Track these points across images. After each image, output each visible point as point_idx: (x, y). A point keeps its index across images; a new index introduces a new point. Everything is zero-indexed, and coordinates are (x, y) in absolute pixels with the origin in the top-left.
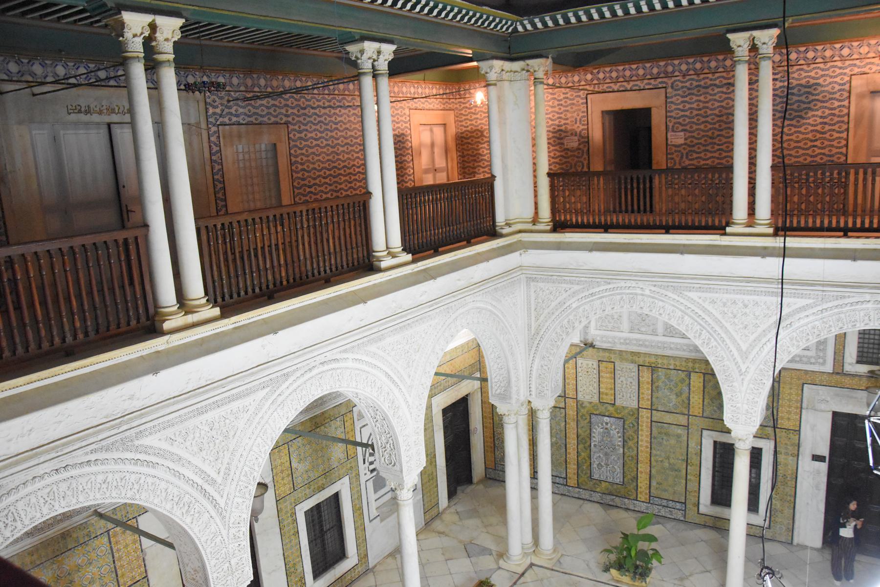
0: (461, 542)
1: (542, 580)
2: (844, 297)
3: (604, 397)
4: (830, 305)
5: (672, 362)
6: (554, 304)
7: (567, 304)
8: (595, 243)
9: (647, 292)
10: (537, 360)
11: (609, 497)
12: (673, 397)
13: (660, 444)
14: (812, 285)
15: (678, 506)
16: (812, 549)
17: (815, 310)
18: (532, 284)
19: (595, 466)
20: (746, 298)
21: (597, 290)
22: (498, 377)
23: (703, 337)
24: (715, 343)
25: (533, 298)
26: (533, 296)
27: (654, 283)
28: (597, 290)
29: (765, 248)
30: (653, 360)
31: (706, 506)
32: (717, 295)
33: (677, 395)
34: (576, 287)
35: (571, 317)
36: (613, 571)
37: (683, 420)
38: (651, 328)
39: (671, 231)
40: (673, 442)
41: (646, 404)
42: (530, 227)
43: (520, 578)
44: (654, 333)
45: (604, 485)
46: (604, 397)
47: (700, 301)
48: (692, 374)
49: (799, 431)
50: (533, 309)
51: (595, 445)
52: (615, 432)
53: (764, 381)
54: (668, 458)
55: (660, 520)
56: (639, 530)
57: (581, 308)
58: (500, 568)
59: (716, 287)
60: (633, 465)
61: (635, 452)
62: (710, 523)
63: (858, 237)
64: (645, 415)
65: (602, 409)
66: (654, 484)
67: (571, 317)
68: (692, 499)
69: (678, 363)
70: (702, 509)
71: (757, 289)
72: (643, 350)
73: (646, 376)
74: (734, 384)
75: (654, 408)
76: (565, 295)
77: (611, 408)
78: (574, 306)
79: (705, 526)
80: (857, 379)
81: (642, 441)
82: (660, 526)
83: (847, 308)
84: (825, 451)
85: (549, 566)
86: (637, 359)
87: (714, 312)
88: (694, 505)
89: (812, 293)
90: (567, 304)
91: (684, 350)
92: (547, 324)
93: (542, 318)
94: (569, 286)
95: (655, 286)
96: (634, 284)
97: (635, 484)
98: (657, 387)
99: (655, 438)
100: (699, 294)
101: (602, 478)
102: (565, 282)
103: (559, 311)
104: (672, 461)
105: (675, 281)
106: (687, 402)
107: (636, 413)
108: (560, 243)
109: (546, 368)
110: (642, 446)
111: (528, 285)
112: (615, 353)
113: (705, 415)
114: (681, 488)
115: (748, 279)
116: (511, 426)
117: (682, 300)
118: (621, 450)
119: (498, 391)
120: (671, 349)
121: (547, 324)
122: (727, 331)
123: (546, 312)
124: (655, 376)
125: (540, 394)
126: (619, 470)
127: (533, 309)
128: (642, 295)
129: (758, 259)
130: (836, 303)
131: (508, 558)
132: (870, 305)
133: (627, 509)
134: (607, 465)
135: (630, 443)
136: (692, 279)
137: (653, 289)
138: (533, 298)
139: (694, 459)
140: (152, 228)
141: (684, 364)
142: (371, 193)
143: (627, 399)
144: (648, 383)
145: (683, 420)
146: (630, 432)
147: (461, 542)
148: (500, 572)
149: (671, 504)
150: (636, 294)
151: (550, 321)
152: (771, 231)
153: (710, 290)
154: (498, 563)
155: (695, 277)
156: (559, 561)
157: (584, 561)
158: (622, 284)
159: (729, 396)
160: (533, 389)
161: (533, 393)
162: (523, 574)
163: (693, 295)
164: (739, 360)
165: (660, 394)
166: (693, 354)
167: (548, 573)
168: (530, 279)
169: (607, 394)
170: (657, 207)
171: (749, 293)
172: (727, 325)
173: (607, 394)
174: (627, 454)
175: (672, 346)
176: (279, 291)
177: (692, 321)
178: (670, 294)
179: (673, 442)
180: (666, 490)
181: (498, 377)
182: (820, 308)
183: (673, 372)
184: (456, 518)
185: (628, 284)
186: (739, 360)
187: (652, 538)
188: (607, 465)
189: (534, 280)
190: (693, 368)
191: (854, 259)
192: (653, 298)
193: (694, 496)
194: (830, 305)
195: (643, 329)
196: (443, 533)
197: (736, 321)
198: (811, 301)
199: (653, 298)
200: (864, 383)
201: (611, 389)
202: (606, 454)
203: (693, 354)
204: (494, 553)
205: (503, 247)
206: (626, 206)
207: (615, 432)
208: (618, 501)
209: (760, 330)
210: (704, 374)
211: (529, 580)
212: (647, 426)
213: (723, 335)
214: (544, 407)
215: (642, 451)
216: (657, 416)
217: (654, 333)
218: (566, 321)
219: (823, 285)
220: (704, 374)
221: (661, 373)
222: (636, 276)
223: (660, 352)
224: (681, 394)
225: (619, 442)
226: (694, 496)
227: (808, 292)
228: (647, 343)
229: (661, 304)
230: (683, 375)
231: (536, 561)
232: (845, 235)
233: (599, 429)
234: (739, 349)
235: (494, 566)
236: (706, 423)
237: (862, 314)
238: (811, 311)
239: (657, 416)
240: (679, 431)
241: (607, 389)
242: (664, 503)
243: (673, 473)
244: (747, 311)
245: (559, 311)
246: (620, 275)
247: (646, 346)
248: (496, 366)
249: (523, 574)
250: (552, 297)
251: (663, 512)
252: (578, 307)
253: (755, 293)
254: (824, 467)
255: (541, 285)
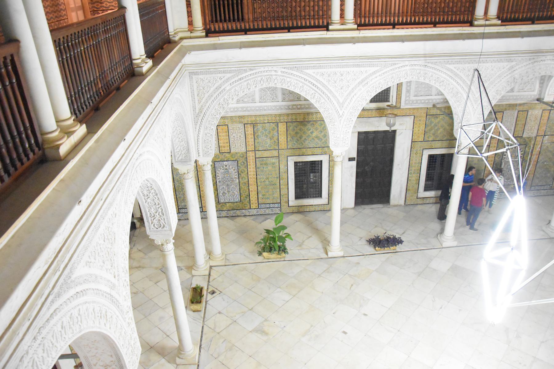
0: (156, 268)
1: (223, 273)
2: (396, 64)
3: (223, 149)
4: (388, 69)
5: (266, 118)
6: (212, 89)
7: (222, 88)
8: (241, 42)
9: (279, 73)
10: (202, 131)
11: (232, 212)
12: (268, 141)
13: (262, 171)
14: (379, 58)
15: (276, 205)
16: (352, 209)
17: (380, 73)
18: (194, 77)
19: (221, 194)
20: (342, 70)
21: (244, 75)
22: (179, 148)
23: (316, 97)
24: (323, 101)
25: (195, 87)
26: (195, 85)
27: (284, 66)
28: (244, 75)
29: (353, 38)
30: (254, 119)
31: (292, 201)
32: (325, 70)
33: (271, 139)
34: (229, 75)
35: (226, 97)
36: (265, 254)
37: (275, 153)
38: (251, 98)
39: (248, 33)
40: (270, 168)
41: (251, 148)
42: (188, 34)
43: (209, 278)
44: (253, 101)
45: (228, 205)
46: (223, 149)
47: (314, 75)
48: (279, 124)
49: (412, 142)
50: (196, 95)
51: (220, 182)
52: (232, 170)
53: (352, 119)
54: (268, 178)
55: (268, 217)
56: (276, 225)
57: (233, 90)
58: (193, 276)
59: (323, 65)
60: (246, 188)
61: (247, 180)
62: (296, 210)
63: (384, 29)
64: (251, 155)
65: (222, 157)
66: (260, 196)
67: (226, 97)
68: (284, 199)
69: (270, 119)
70: (291, 204)
71: (348, 64)
72: (246, 113)
73: (250, 130)
74: (335, 124)
75: (256, 149)
76: (220, 82)
77: (227, 155)
78: (228, 88)
79: (293, 213)
80: (370, 111)
81: (250, 171)
82: (269, 220)
83: (397, 70)
84: (354, 155)
85: (223, 264)
86: (243, 120)
87: (323, 81)
88: (286, 202)
89: (379, 63)
90: (222, 88)
91: (274, 110)
92: (208, 104)
93: (203, 101)
94: (223, 75)
95: (285, 68)
96: (270, 68)
97: (248, 199)
98: (258, 136)
99: (258, 168)
100: (313, 70)
101: (226, 201)
102: (220, 72)
103: (216, 94)
104: (270, 179)
105: (297, 65)
106: (277, 141)
107: (245, 156)
108: (214, 44)
109: (209, 135)
110: (250, 175)
111: (191, 78)
112: (228, 119)
113: (289, 147)
114: (277, 195)
115: (343, 58)
116: (190, 180)
117: (303, 76)
118: (238, 180)
119: (180, 158)
120: (265, 110)
121: (208, 104)
122: (331, 92)
123: (206, 96)
124: (255, 129)
125: (206, 154)
126: (237, 193)
127: (196, 95)
128: (276, 75)
129: (350, 45)
130: (391, 68)
131: (198, 268)
132: (408, 68)
133: (245, 216)
134: (229, 192)
135: (243, 175)
136: (309, 61)
137: (283, 70)
138: (195, 87)
139: (284, 176)
140: (22, 44)
141: (274, 118)
142: (125, 8)
143: (238, 147)
144: (251, 134)
145: (275, 153)
146: (242, 168)
147: (156, 268)
148: (194, 278)
149: (272, 206)
150: (271, 75)
151: (209, 102)
152: (204, 34)
153: (320, 67)
154: (191, 273)
155: (310, 59)
156: (226, 259)
157: (241, 254)
158: (262, 69)
159: (332, 131)
160: (201, 152)
161: (201, 154)
162: (210, 274)
163: (309, 71)
164: (338, 108)
165: (260, 140)
166: (280, 111)
167: (224, 268)
168: (191, 74)
169: (224, 147)
170: (246, 17)
171: (343, 67)
172: (331, 88)
173: (224, 147)
174: (242, 182)
175: (265, 108)
176: (102, 100)
177: (309, 88)
178: (295, 73)
179: (270, 168)
180: (268, 198)
181: (179, 148)
182: (383, 72)
183: (267, 125)
184: (141, 254)
185: (266, 69)
186: (338, 108)
187: (284, 228)
188: (229, 192)
189: (196, 73)
190: (280, 120)
191: (403, 41)
192: (283, 76)
193: (286, 197)
194: (388, 69)
195: (246, 100)
196: (140, 267)
197: (336, 85)
198: (379, 68)
199: (283, 76)
200: (374, 113)
201: (227, 143)
202: (228, 185)
203: (280, 111)
204: (183, 268)
205: (545, 31)
206: (229, 17)
207: (232, 170)
208: (238, 213)
209: (350, 89)
210: (286, 122)
211: (216, 277)
212: (253, 162)
213: (329, 95)
214: (206, 162)
215: (251, 178)
216: (259, 154)
217: (253, 101)
218: (222, 100)
219: (384, 58)
220: (286, 122)
221: (259, 126)
222: (271, 63)
223: (258, 113)
224: (273, 137)
225: (235, 175)
226: (286, 197)
227: (377, 63)
228: (249, 109)
229: (288, 79)
230: (273, 125)
231: (212, 263)
232: (435, 26)
233: (221, 171)
234: (338, 102)
235: (189, 276)
236: (289, 152)
237: (404, 73)
238: (378, 74)
239: (259, 154)
240: (273, 160)
241: (224, 143)
242: (268, 206)
243: (272, 187)
244: (343, 78)
245: (216, 94)
246: (260, 63)
247: (248, 111)
248: (177, 140)
249: (210, 274)
250: (210, 84)
251: (268, 211)
252: (230, 90)
253: (347, 66)
254: (354, 163)
255: (201, 76)
